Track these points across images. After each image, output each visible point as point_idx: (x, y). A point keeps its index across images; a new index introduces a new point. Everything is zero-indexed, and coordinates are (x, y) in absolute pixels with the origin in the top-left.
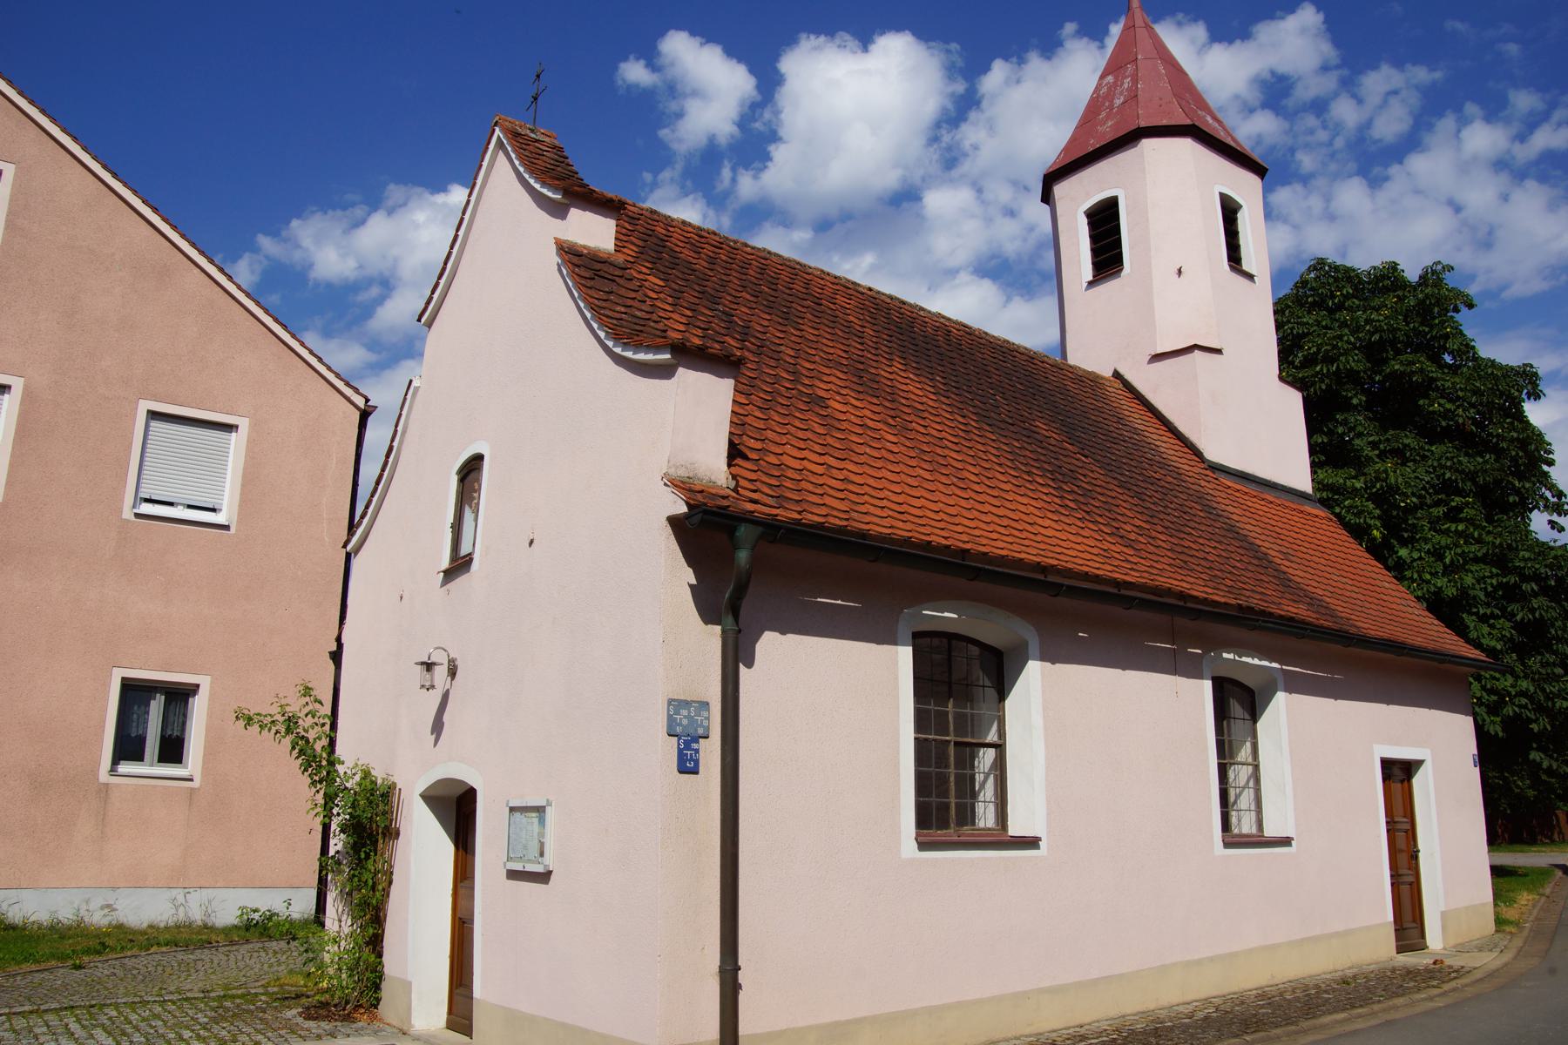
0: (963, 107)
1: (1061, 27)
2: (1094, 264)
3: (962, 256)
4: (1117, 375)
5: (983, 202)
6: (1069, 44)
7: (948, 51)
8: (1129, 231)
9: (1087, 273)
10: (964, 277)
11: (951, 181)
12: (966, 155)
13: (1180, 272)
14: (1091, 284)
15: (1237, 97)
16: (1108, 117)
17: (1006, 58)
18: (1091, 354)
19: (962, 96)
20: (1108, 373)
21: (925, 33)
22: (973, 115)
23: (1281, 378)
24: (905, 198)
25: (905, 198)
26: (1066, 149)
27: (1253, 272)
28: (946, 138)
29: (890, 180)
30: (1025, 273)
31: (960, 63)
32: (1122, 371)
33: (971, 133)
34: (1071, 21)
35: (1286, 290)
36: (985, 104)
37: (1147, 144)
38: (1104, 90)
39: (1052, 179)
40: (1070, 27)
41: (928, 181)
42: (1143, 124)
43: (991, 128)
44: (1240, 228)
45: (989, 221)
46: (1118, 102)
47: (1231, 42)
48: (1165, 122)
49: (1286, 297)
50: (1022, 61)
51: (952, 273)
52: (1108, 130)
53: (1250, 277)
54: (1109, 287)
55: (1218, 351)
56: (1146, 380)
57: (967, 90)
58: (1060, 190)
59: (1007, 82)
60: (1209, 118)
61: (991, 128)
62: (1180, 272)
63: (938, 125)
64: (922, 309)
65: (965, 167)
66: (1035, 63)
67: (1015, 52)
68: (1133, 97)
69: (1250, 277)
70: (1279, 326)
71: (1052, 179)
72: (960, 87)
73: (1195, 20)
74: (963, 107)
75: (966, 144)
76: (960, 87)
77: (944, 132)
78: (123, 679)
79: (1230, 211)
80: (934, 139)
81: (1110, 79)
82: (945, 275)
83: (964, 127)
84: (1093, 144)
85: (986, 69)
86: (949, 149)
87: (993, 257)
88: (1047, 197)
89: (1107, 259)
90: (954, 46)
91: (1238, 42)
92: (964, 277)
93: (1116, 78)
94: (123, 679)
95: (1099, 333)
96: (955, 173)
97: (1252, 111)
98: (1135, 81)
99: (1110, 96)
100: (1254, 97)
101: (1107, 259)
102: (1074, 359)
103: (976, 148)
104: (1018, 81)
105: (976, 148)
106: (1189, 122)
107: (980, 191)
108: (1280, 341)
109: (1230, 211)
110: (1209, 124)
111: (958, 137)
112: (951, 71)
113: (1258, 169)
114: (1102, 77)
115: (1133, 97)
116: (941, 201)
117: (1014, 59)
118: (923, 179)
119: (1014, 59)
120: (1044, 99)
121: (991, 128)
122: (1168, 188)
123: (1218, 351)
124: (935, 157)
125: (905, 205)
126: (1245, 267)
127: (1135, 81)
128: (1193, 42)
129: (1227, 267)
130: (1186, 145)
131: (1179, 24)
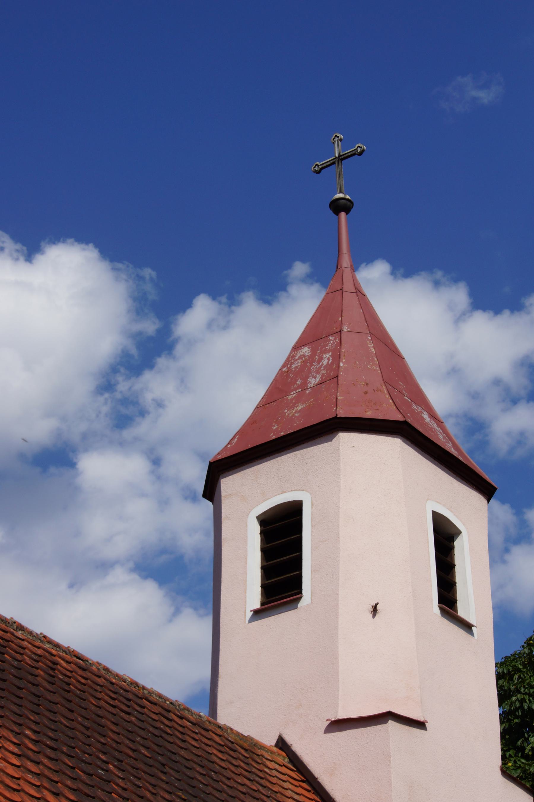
0: (149, 350)
1: (289, 266)
2: (264, 587)
3: (122, 546)
4: (282, 744)
5: (159, 478)
6: (294, 290)
7: (140, 278)
8: (314, 548)
9: (254, 598)
10: (119, 575)
11: (122, 444)
12: (143, 413)
13: (375, 610)
14: (258, 614)
15: (497, 382)
16: (298, 399)
17: (214, 296)
18: (249, 712)
19: (150, 339)
20: (270, 741)
21: (114, 250)
22: (162, 361)
23: (505, 772)
24: (56, 459)
25: (56, 459)
26: (242, 433)
27: (471, 620)
28: (123, 386)
29: (40, 431)
30: (193, 582)
31: (153, 295)
32: (289, 739)
33: (156, 385)
34: (303, 261)
35: (516, 645)
36: (179, 349)
37: (345, 439)
38: (298, 363)
39: (220, 468)
40: (300, 269)
41: (89, 441)
42: (342, 413)
43: (183, 382)
44: (457, 560)
45: (163, 503)
46: (313, 381)
47: (497, 311)
48: (369, 414)
49: (515, 657)
50: (233, 301)
51: (104, 566)
52: (296, 415)
53: (467, 627)
54: (281, 621)
55: (420, 725)
56: (319, 754)
57: (158, 331)
58: (228, 484)
59: (210, 325)
60: (425, 416)
61: (182, 381)
62: (375, 610)
63: (114, 369)
64: (21, 627)
65: (142, 428)
66: (250, 307)
67: (228, 293)
68: (333, 378)
69: (467, 627)
70: (503, 696)
71: (220, 468)
72: (150, 326)
73: (456, 280)
74: (149, 350)
75: (148, 397)
76: (150, 326)
77: (120, 378)
78: (258, 518)
79: (445, 537)
80: (106, 386)
81: (306, 351)
82: (85, 570)
83: (147, 376)
84: (277, 431)
85: (185, 305)
86: (125, 401)
87: (164, 551)
88: (211, 491)
89: (282, 583)
90: (148, 272)
91: (507, 313)
92: (119, 575)
93: (314, 352)
94: (258, 518)
95: (262, 685)
96: (127, 434)
97: (515, 401)
98: (337, 357)
99: (304, 372)
100: (518, 383)
101: (282, 583)
102: (224, 717)
103: (160, 404)
104: (225, 328)
105: (160, 404)
106: (399, 417)
107: (156, 462)
108: (504, 718)
109: (445, 537)
110: (425, 423)
111: (137, 387)
112: (141, 305)
113: (487, 490)
114: (297, 347)
115: (333, 378)
116: (102, 469)
117: (224, 299)
118: (84, 436)
119: (224, 299)
120: (237, 357)
121: (183, 382)
122: (368, 501)
123: (420, 725)
124: (105, 409)
125: (52, 470)
126: (462, 612)
127: (337, 357)
128: (450, 307)
129: (437, 610)
130: (394, 447)
131: (437, 284)
